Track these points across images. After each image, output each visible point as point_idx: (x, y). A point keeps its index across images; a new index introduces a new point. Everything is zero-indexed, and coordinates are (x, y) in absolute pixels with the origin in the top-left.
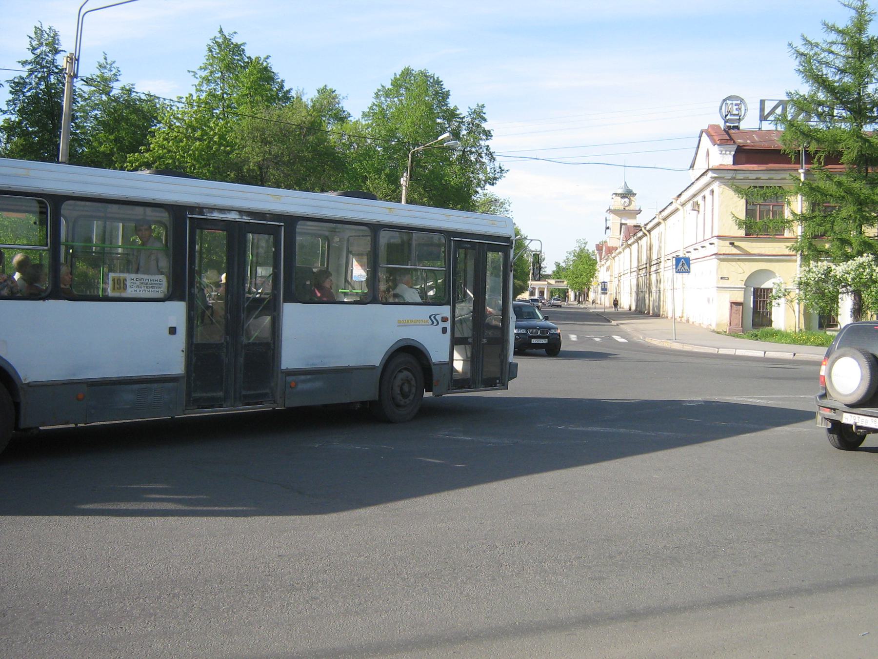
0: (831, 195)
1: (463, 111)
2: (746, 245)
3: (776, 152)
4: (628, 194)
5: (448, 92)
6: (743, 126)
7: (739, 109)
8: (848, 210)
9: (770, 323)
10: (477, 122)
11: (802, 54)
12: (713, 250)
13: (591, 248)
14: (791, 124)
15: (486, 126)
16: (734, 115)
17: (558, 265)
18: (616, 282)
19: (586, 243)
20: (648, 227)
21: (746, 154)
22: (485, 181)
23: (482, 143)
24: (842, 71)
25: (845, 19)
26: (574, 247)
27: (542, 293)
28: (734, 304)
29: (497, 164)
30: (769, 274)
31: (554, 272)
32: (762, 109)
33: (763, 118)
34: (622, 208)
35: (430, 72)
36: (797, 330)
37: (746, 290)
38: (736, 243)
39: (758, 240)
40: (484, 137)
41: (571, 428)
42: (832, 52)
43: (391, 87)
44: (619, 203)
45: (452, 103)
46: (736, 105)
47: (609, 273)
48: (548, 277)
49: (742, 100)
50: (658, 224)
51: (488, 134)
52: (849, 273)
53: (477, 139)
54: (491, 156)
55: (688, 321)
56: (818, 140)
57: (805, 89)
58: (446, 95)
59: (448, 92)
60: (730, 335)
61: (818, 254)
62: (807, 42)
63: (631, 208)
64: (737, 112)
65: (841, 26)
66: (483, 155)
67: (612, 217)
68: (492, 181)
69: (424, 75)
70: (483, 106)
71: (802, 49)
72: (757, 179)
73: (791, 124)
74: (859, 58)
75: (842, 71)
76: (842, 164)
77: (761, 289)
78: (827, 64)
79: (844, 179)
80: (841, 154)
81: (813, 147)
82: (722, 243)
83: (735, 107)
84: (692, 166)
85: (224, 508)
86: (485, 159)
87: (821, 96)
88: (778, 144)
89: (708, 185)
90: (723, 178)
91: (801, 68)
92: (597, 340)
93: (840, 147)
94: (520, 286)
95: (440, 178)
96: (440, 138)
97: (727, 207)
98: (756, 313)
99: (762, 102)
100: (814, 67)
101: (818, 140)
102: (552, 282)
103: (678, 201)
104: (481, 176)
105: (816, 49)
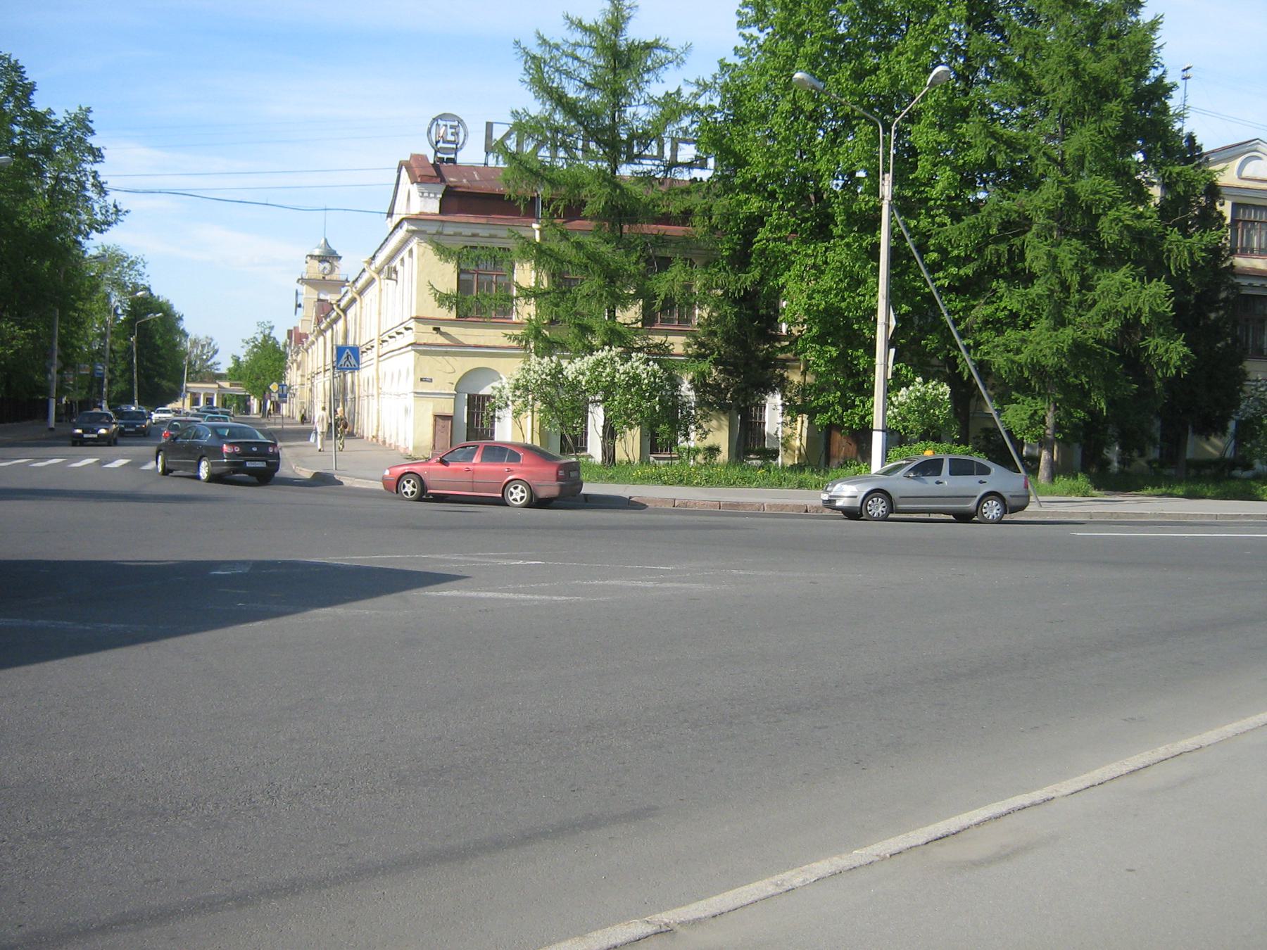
0: (570, 262)
3: (499, 197)
4: (329, 257)
5: (33, 84)
6: (463, 158)
7: (456, 134)
8: (591, 284)
9: (585, 449)
10: (79, 134)
11: (534, 58)
12: (409, 337)
13: (281, 338)
14: (512, 157)
15: (93, 141)
16: (449, 142)
19: (271, 328)
20: (343, 304)
21: (461, 198)
23: (88, 167)
24: (589, 86)
25: (595, 9)
26: (253, 332)
27: (209, 401)
28: (437, 417)
29: (110, 200)
30: (490, 374)
32: (489, 135)
33: (489, 150)
34: (321, 276)
37: (456, 397)
38: (443, 329)
39: (475, 324)
40: (91, 158)
41: (709, 587)
42: (577, 58)
44: (316, 269)
45: (40, 103)
46: (452, 127)
47: (300, 372)
48: (221, 377)
49: (460, 121)
50: (353, 301)
51: (97, 154)
52: (583, 374)
53: (78, 162)
54: (101, 189)
55: (384, 442)
56: (553, 183)
57: (536, 107)
58: (30, 89)
59: (33, 84)
62: (544, 42)
63: (334, 277)
64: (452, 138)
65: (588, 22)
66: (88, 186)
67: (303, 289)
68: (101, 226)
70: (89, 110)
71: (538, 52)
72: (474, 235)
73: (512, 157)
74: (614, 69)
75: (589, 86)
76: (585, 218)
77: (479, 396)
78: (569, 75)
79: (588, 240)
80: (583, 204)
81: (543, 192)
82: (423, 327)
83: (450, 131)
84: (390, 214)
87: (559, 117)
89: (405, 242)
90: (424, 232)
91: (527, 78)
94: (171, 389)
97: (424, 276)
99: (489, 126)
100: (546, 76)
101: (553, 183)
102: (226, 385)
103: (373, 267)
105: (555, 52)
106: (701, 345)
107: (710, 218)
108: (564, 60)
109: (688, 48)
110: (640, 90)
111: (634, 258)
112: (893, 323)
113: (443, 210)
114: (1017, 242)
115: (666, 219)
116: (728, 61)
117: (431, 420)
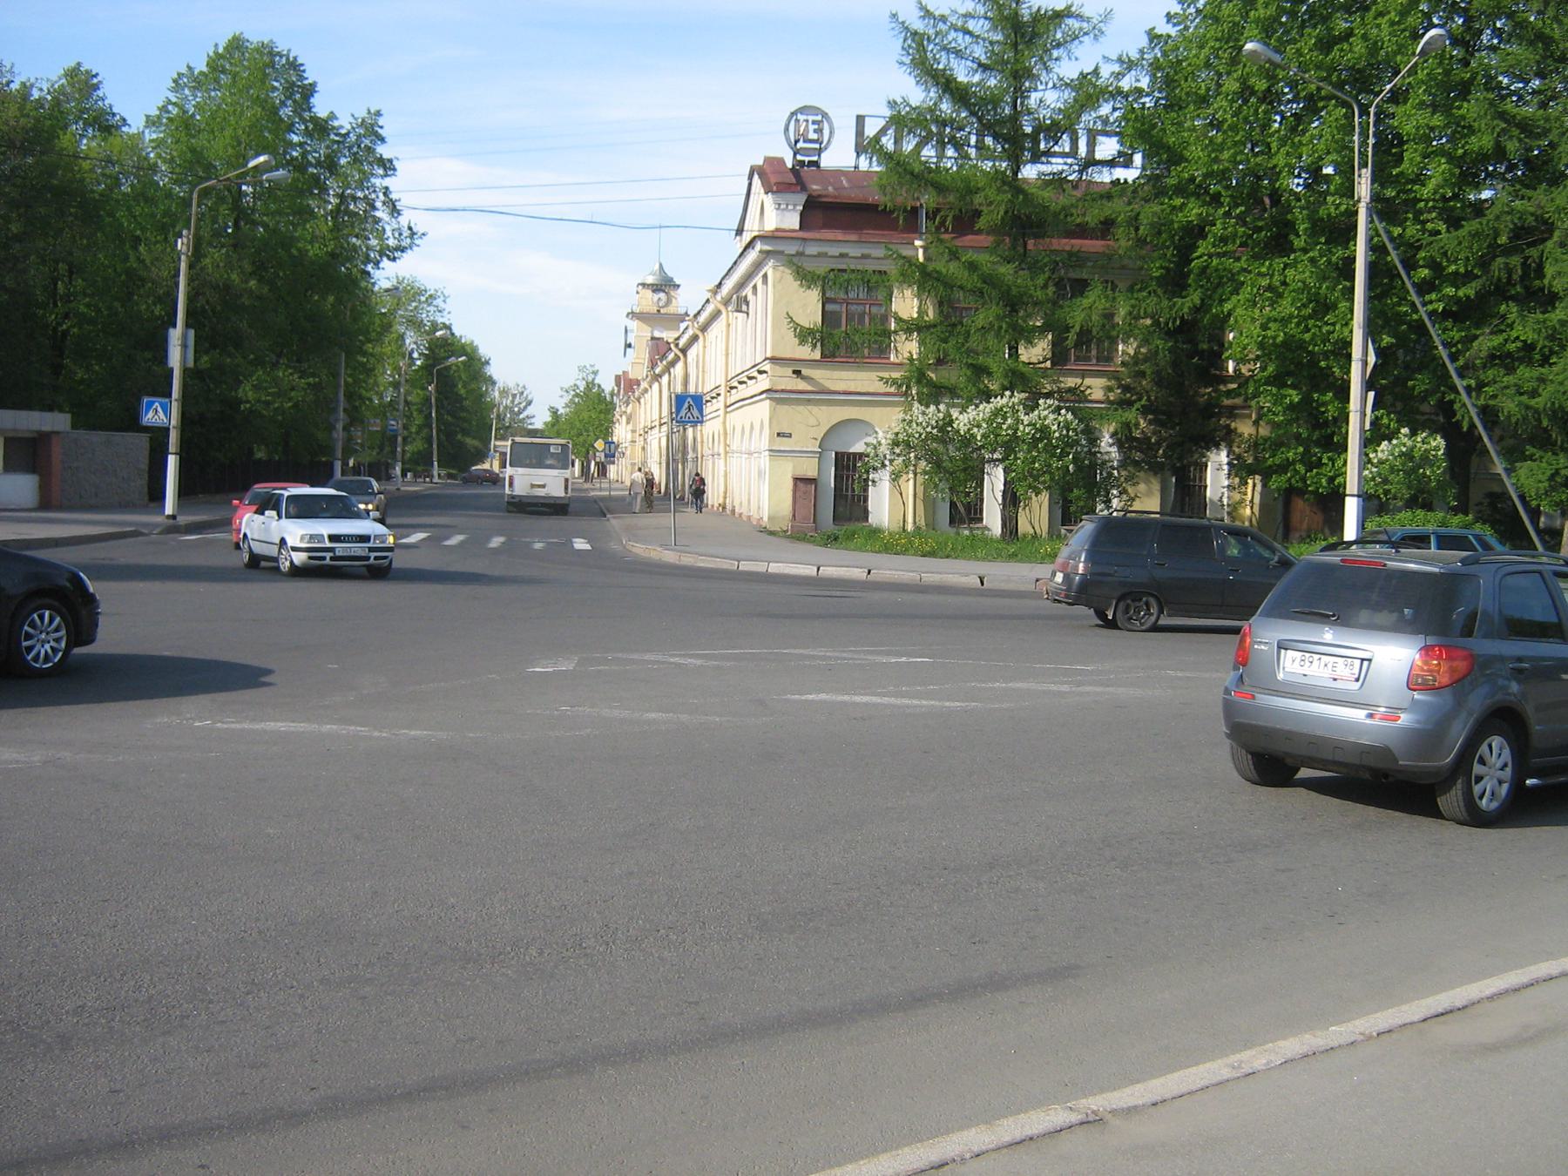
1: (344, 122)
2: (817, 374)
4: (664, 285)
7: (819, 131)
10: (367, 142)
11: (915, 33)
12: (764, 383)
13: (608, 385)
15: (383, 151)
17: (554, 412)
18: (640, 445)
19: (595, 373)
20: (682, 343)
22: (382, 254)
23: (377, 182)
26: (572, 378)
28: (799, 481)
29: (404, 220)
31: (546, 424)
32: (860, 132)
35: (281, 47)
36: (910, 527)
38: (804, 372)
40: (381, 172)
42: (967, 32)
43: (205, 69)
44: (649, 301)
45: (321, 106)
46: (814, 122)
47: (630, 427)
49: (825, 115)
50: (695, 338)
51: (388, 166)
52: (979, 426)
53: (366, 177)
55: (733, 511)
57: (916, 94)
58: (309, 91)
59: (313, 85)
60: (784, 535)
61: (935, 393)
62: (927, 14)
63: (671, 309)
64: (815, 136)
66: (378, 204)
67: (634, 325)
68: (392, 253)
69: (268, 53)
72: (842, 256)
75: (984, 67)
76: (979, 232)
77: (849, 454)
78: (958, 53)
79: (983, 258)
81: (927, 199)
83: (812, 127)
85: (1053, 687)
86: (382, 213)
87: (946, 107)
88: (875, 197)
92: (538, 546)
93: (978, 199)
95: (287, 242)
96: (252, 164)
97: (784, 304)
98: (837, 501)
99: (860, 120)
100: (930, 55)
101: (940, 188)
103: (719, 298)
104: (374, 242)
105: (941, 26)
106: (1126, 389)
107: (1137, 229)
108: (953, 34)
109: (1107, 16)
110: (1048, 70)
111: (1040, 281)
112: (1372, 359)
113: (804, 224)
114: (1534, 252)
115: (1082, 231)
116: (1158, 31)
117: (789, 484)
